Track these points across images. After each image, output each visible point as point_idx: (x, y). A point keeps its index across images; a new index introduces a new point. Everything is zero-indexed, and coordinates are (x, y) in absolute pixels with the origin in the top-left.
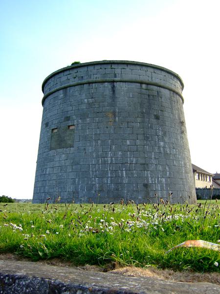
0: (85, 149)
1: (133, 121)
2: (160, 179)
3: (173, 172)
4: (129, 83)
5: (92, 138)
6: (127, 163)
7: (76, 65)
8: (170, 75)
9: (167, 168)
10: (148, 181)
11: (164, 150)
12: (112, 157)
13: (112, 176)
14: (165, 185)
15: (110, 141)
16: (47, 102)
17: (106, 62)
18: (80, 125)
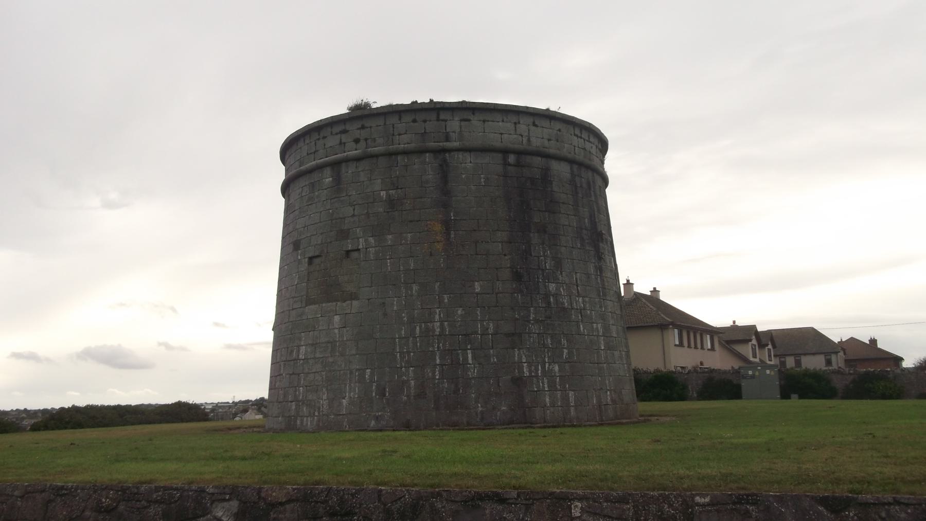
2: (547, 365)
9: (564, 342)
12: (442, 322)
17: (464, 106)
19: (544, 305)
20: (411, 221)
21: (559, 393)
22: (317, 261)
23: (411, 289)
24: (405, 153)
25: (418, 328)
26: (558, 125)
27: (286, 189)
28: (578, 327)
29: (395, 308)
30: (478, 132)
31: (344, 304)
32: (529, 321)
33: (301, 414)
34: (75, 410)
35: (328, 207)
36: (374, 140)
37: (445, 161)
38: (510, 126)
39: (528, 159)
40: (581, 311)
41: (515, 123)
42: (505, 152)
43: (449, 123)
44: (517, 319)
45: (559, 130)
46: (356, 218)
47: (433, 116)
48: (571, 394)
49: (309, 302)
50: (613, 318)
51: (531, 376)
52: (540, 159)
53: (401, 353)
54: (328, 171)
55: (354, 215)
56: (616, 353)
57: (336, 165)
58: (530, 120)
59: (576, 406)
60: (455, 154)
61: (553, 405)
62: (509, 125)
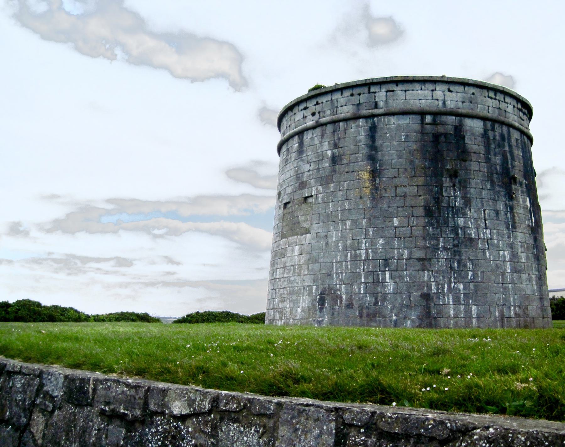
0: (326, 236)
1: (406, 184)
2: (453, 284)
3: (483, 272)
4: (401, 116)
5: (337, 216)
6: (393, 258)
7: (318, 92)
8: (485, 92)
9: (469, 265)
10: (429, 287)
12: (367, 250)
13: (367, 281)
14: (462, 296)
15: (365, 220)
18: (320, 196)
19: (452, 236)
20: (347, 172)
21: (462, 307)
22: (289, 206)
23: (345, 224)
24: (345, 120)
25: (349, 254)
26: (471, 90)
28: (485, 254)
29: (334, 239)
30: (402, 98)
31: (302, 237)
32: (438, 249)
33: (276, 318)
34: (132, 314)
35: (296, 165)
36: (324, 112)
37: (374, 123)
38: (428, 93)
39: (444, 118)
40: (488, 241)
41: (432, 91)
42: (422, 114)
43: (377, 94)
44: (428, 247)
45: (473, 94)
46: (311, 173)
47: (366, 89)
48: (474, 308)
49: (283, 236)
50: (521, 246)
52: (454, 118)
53: (337, 273)
54: (296, 139)
55: (309, 170)
56: (524, 276)
57: (300, 133)
58: (445, 87)
59: (478, 318)
61: (456, 316)
62: (426, 92)
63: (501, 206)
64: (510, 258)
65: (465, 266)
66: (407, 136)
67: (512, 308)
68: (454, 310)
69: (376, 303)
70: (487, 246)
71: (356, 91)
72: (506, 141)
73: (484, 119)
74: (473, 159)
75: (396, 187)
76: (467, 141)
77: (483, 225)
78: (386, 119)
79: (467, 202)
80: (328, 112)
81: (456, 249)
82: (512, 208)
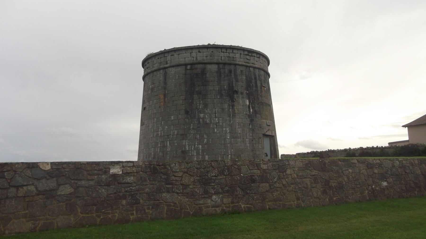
2: (196, 146)
6: (170, 135)
9: (205, 136)
11: (203, 121)
12: (161, 131)
16: (146, 79)
17: (175, 49)
27: (144, 78)
32: (190, 129)
37: (166, 72)
38: (188, 54)
39: (196, 66)
42: (186, 65)
43: (167, 57)
45: (212, 52)
47: (163, 56)
51: (189, 150)
58: (197, 50)
60: (169, 69)
63: (226, 106)
64: (230, 131)
65: (203, 136)
66: (179, 77)
67: (230, 156)
68: (197, 158)
69: (163, 156)
70: (215, 126)
71: (159, 57)
72: (233, 73)
73: (218, 64)
74: (210, 84)
75: (173, 101)
76: (208, 76)
77: (214, 116)
78: (170, 69)
79: (206, 106)
80: (151, 67)
81: (199, 129)
82: (233, 106)
